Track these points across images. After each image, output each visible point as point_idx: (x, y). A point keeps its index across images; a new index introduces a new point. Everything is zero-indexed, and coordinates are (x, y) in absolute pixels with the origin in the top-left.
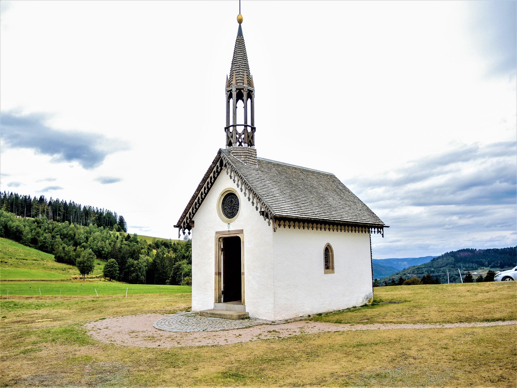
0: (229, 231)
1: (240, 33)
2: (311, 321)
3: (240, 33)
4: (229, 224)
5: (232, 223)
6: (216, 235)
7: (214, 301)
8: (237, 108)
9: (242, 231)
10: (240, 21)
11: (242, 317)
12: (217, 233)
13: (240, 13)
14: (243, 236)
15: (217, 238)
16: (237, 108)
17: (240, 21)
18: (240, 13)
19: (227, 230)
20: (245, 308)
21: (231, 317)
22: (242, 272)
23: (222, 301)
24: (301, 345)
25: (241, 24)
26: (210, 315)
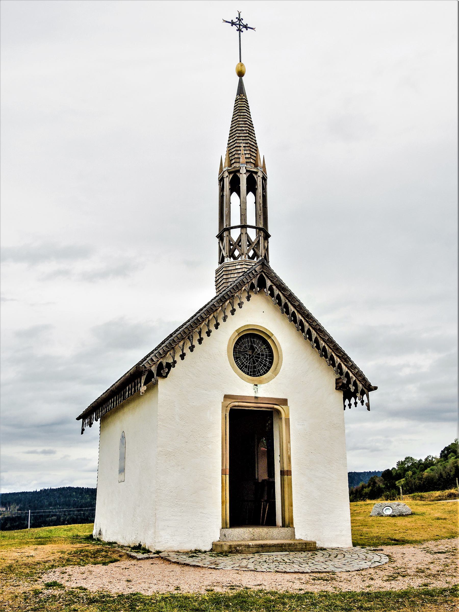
0: (256, 398)
1: (241, 90)
2: (192, 557)
3: (241, 90)
4: (256, 385)
5: (262, 385)
6: (224, 400)
7: (220, 526)
8: (231, 203)
9: (284, 402)
10: (241, 74)
11: (375, 541)
12: (227, 397)
13: (240, 61)
14: (288, 410)
15: (227, 407)
16: (231, 203)
17: (241, 74)
18: (240, 61)
19: (253, 395)
20: (294, 532)
21: (306, 546)
22: (228, 476)
23: (229, 526)
24: (424, 574)
25: (243, 78)
26: (254, 550)
